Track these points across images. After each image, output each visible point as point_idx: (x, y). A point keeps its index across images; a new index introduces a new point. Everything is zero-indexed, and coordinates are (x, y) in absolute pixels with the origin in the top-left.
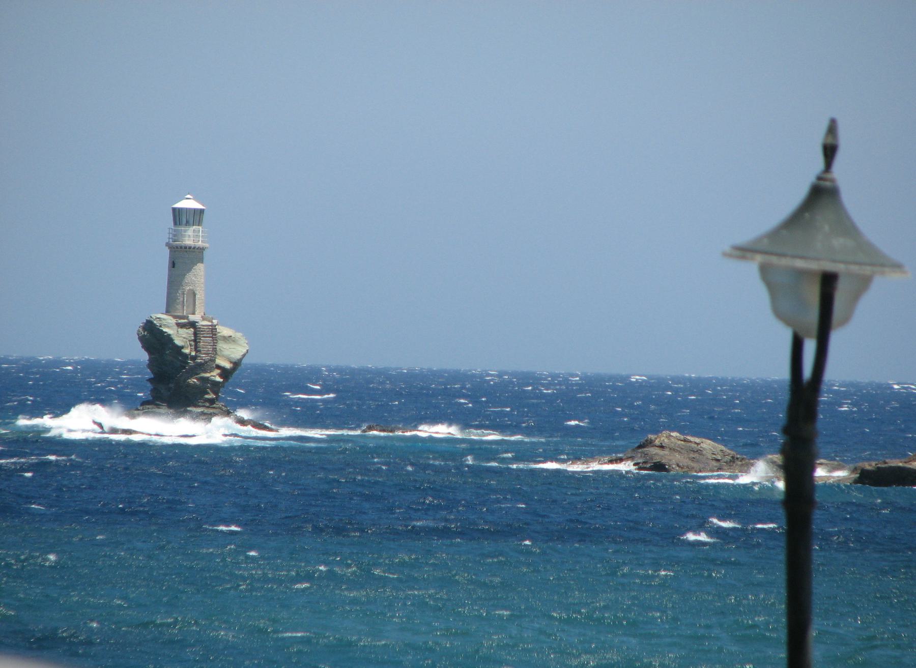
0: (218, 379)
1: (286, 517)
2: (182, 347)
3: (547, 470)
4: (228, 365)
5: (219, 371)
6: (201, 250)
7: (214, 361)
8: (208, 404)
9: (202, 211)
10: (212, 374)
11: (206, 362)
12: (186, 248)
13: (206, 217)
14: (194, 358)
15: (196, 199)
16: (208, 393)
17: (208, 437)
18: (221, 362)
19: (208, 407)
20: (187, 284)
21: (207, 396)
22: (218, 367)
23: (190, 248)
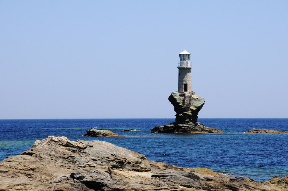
0: (190, 114)
1: (185, 153)
2: (179, 103)
3: (180, 126)
4: (194, 109)
5: (191, 111)
6: (190, 69)
7: (189, 107)
8: (186, 123)
9: (189, 55)
10: (188, 112)
11: (185, 108)
12: (183, 68)
13: (191, 57)
14: (183, 106)
15: (187, 51)
16: (187, 119)
17: (20, 182)
18: (192, 107)
19: (187, 124)
20: (184, 81)
21: (186, 120)
22: (191, 109)
23: (185, 68)
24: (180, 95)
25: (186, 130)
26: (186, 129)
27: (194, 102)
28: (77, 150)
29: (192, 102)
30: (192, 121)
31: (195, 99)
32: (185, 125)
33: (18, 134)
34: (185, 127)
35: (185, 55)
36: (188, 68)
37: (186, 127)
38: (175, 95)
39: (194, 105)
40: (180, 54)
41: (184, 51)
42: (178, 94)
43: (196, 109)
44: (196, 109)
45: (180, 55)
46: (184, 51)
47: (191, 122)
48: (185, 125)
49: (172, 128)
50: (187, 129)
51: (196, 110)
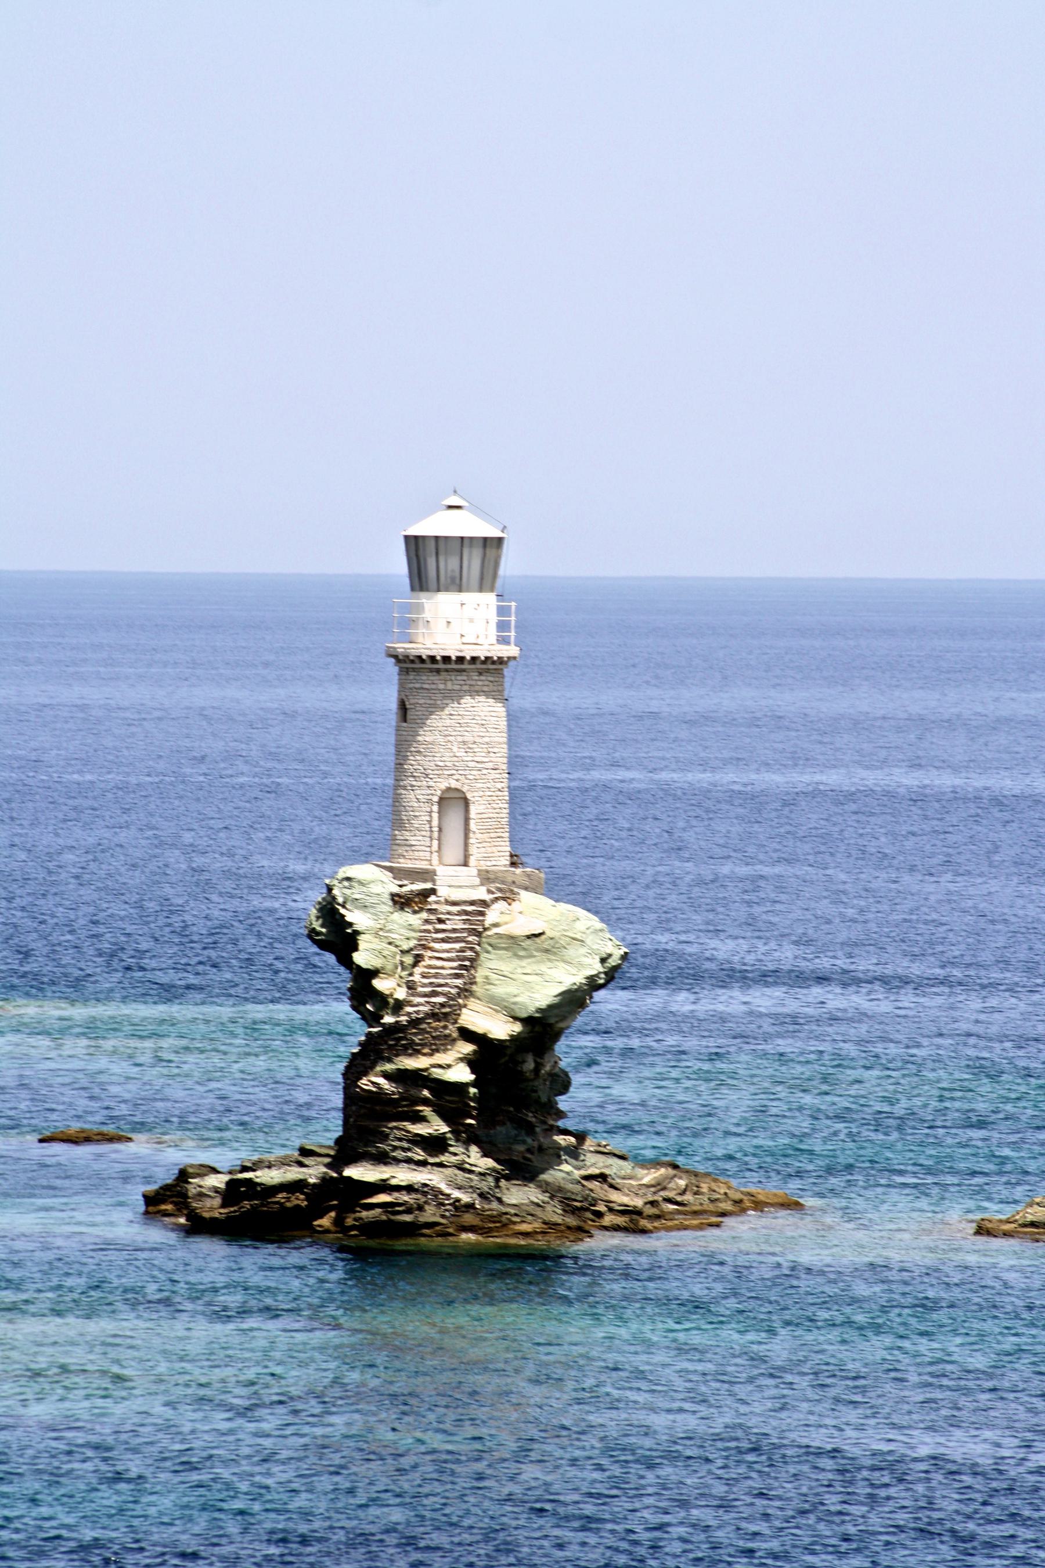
0: (462, 1074)
4: (501, 1029)
5: (468, 1048)
9: (500, 541)
10: (440, 1058)
22: (467, 1035)
24: (393, 896)
25: (407, 1218)
26: (409, 1211)
27: (506, 967)
28: (911, 1466)
29: (493, 966)
30: (471, 1138)
31: (513, 944)
32: (402, 1175)
33: (296, 1283)
34: (405, 1197)
35: (433, 543)
36: (474, 659)
37: (409, 1188)
38: (356, 893)
39: (501, 990)
40: (407, 538)
41: (450, 507)
42: (376, 889)
43: (517, 1028)
44: (517, 1028)
45: (415, 545)
46: (450, 507)
47: (467, 1143)
48: (402, 1175)
49: (299, 1200)
50: (420, 1208)
51: (514, 1039)
